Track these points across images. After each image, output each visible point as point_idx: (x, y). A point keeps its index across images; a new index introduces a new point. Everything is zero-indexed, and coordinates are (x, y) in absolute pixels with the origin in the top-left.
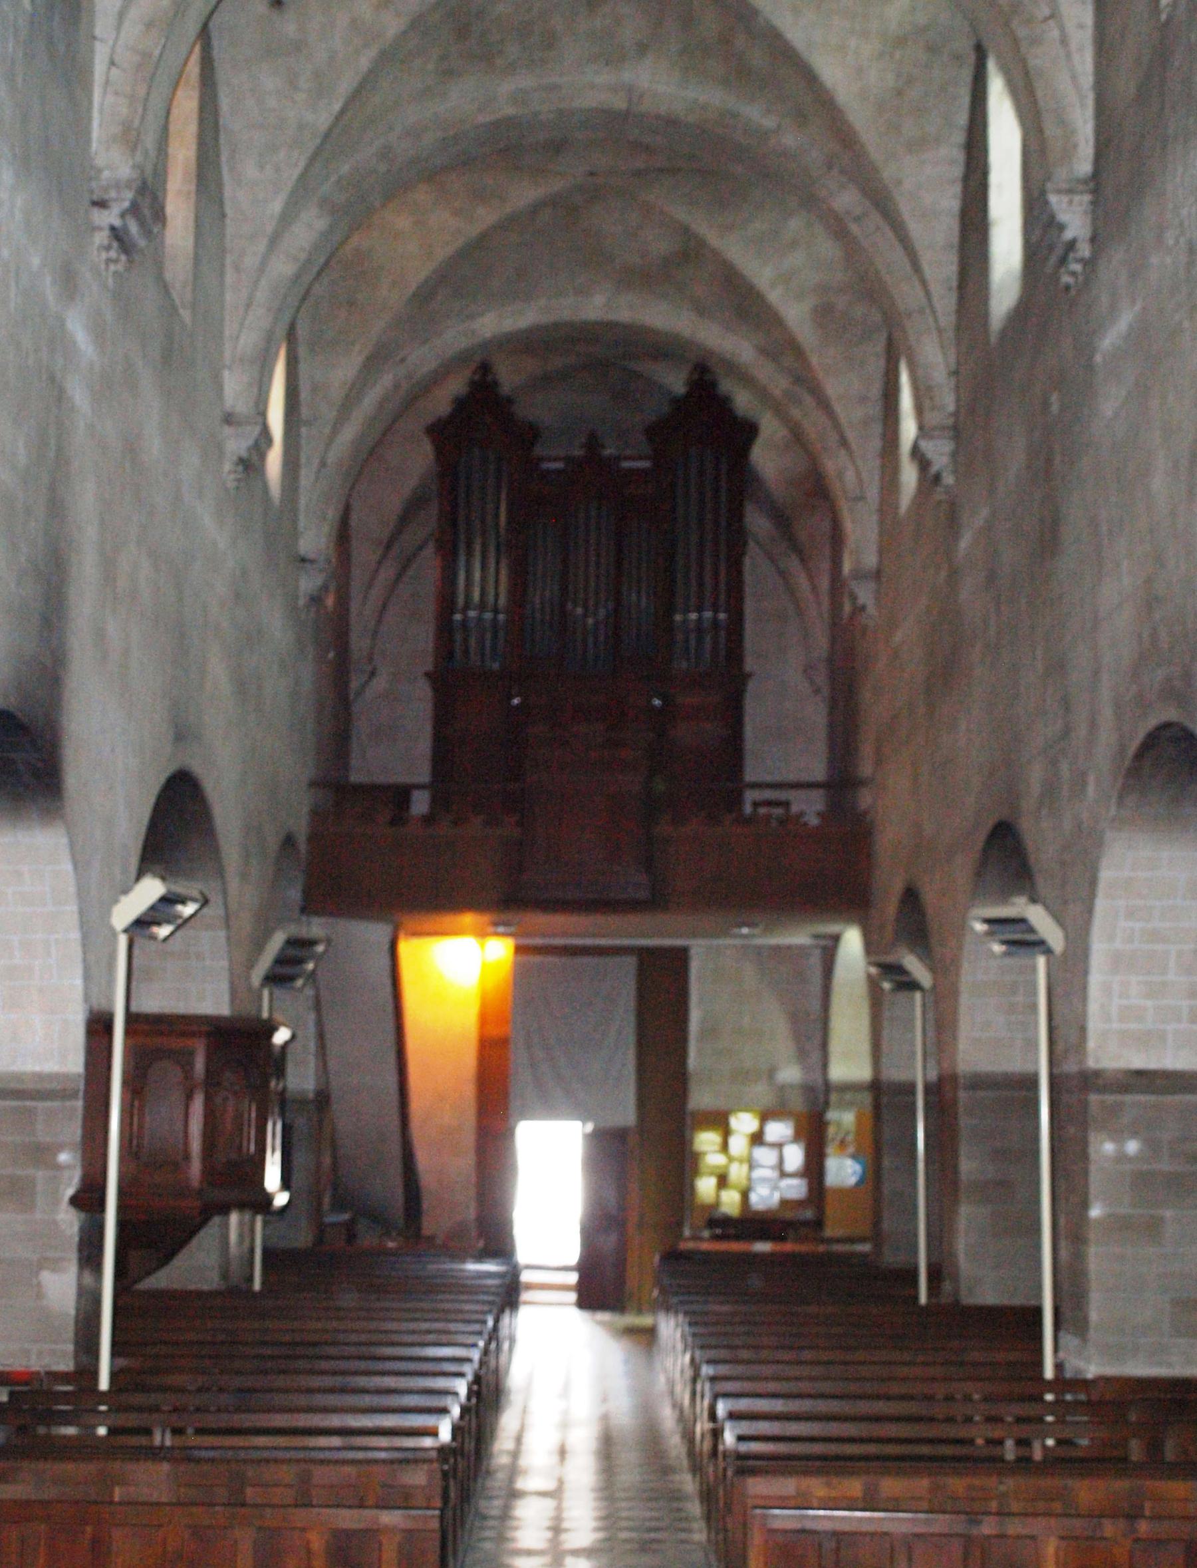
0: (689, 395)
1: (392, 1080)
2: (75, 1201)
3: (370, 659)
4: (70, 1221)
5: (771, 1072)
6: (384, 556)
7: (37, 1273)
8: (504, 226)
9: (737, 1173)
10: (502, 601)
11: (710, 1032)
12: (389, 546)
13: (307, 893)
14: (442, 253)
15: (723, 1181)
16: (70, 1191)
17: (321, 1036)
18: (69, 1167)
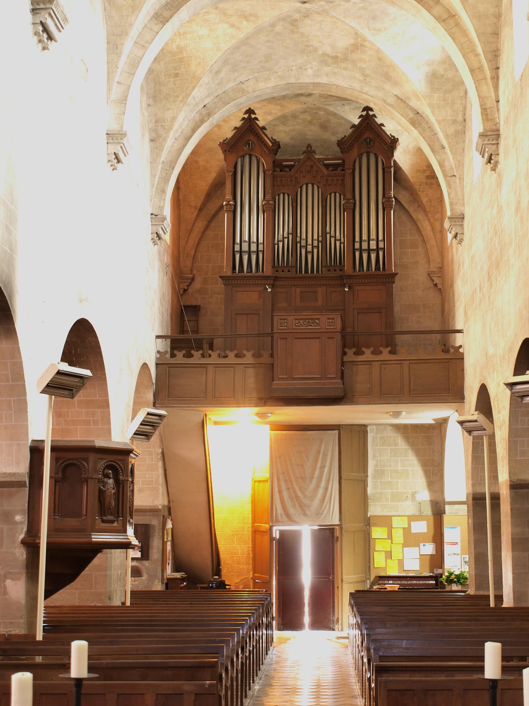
0: (360, 123)
1: (204, 498)
2: (24, 542)
3: (192, 271)
4: (21, 554)
5: (414, 494)
6: (198, 215)
7: (4, 581)
8: (258, 31)
11: (379, 473)
13: (156, 395)
15: (389, 555)
16: (22, 536)
18: (21, 523)
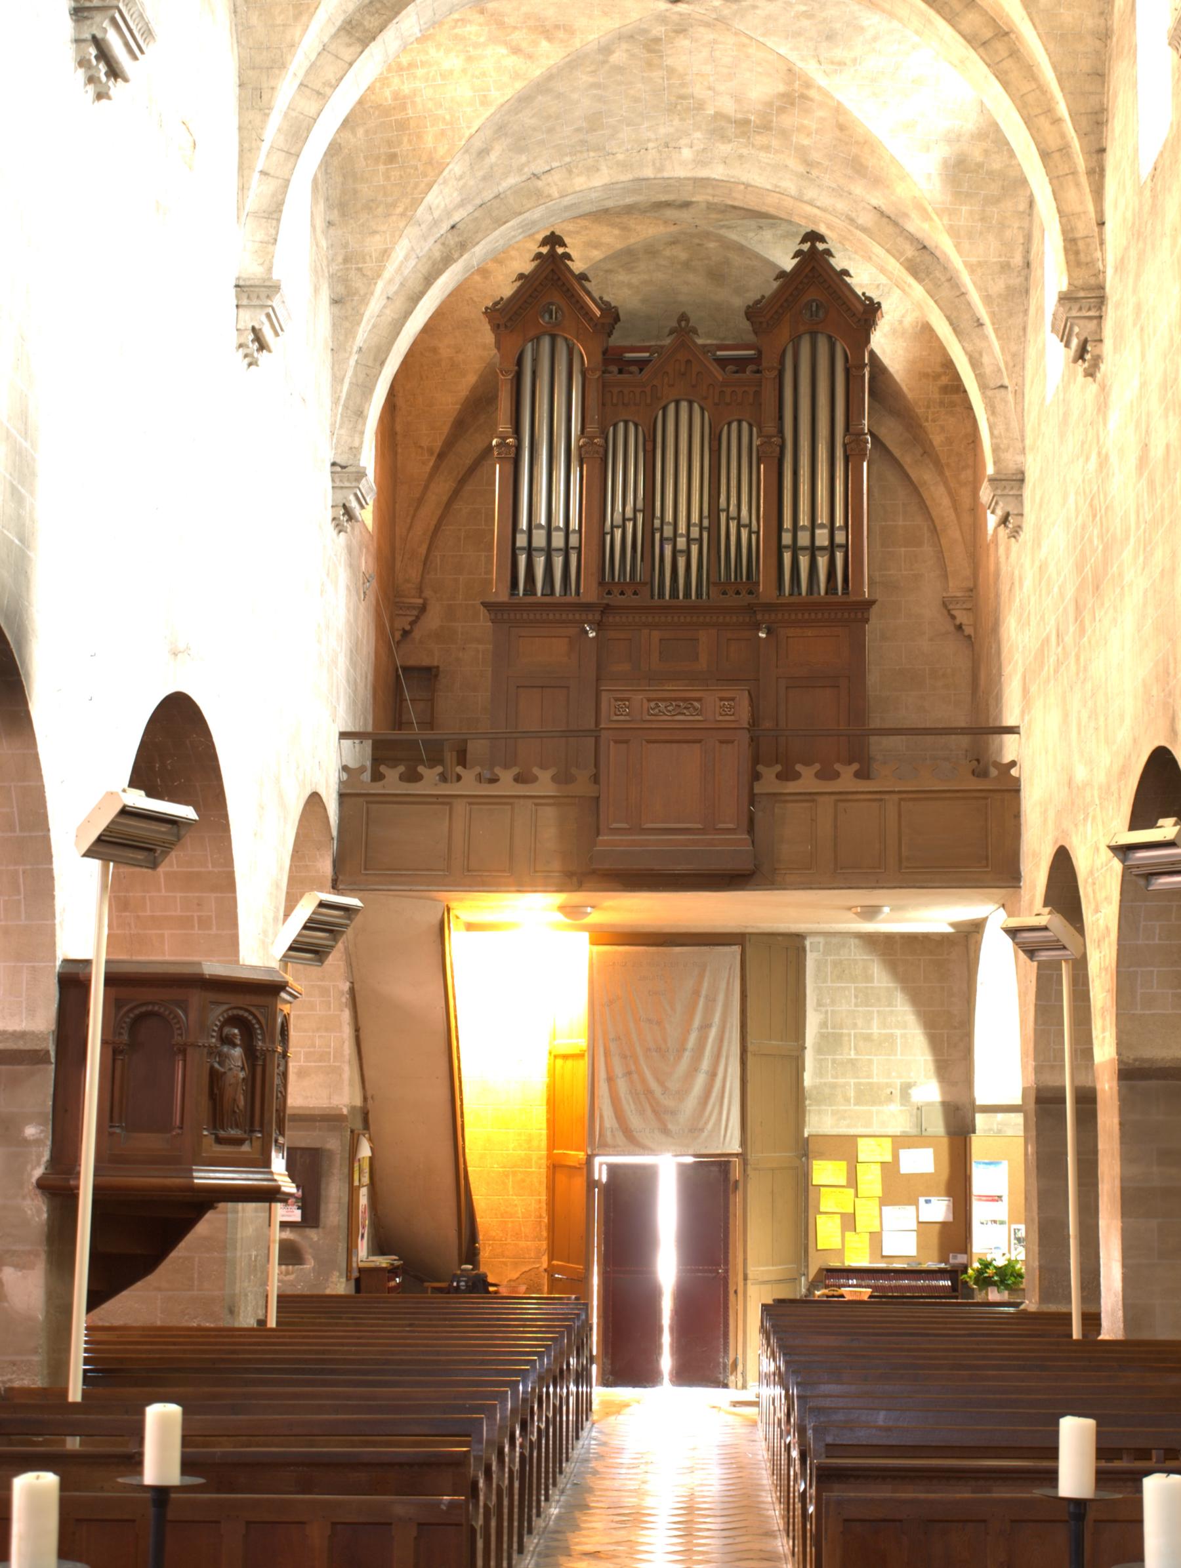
1: (443, 1093)
2: (42, 1185)
3: (420, 590)
4: (36, 1210)
5: (906, 1089)
6: (436, 468)
8: (574, 63)
9: (867, 1221)
10: (574, 524)
12: (441, 456)
14: (499, 97)
15: (849, 1222)
16: (38, 1172)
17: (357, 1030)
18: (38, 1142)
